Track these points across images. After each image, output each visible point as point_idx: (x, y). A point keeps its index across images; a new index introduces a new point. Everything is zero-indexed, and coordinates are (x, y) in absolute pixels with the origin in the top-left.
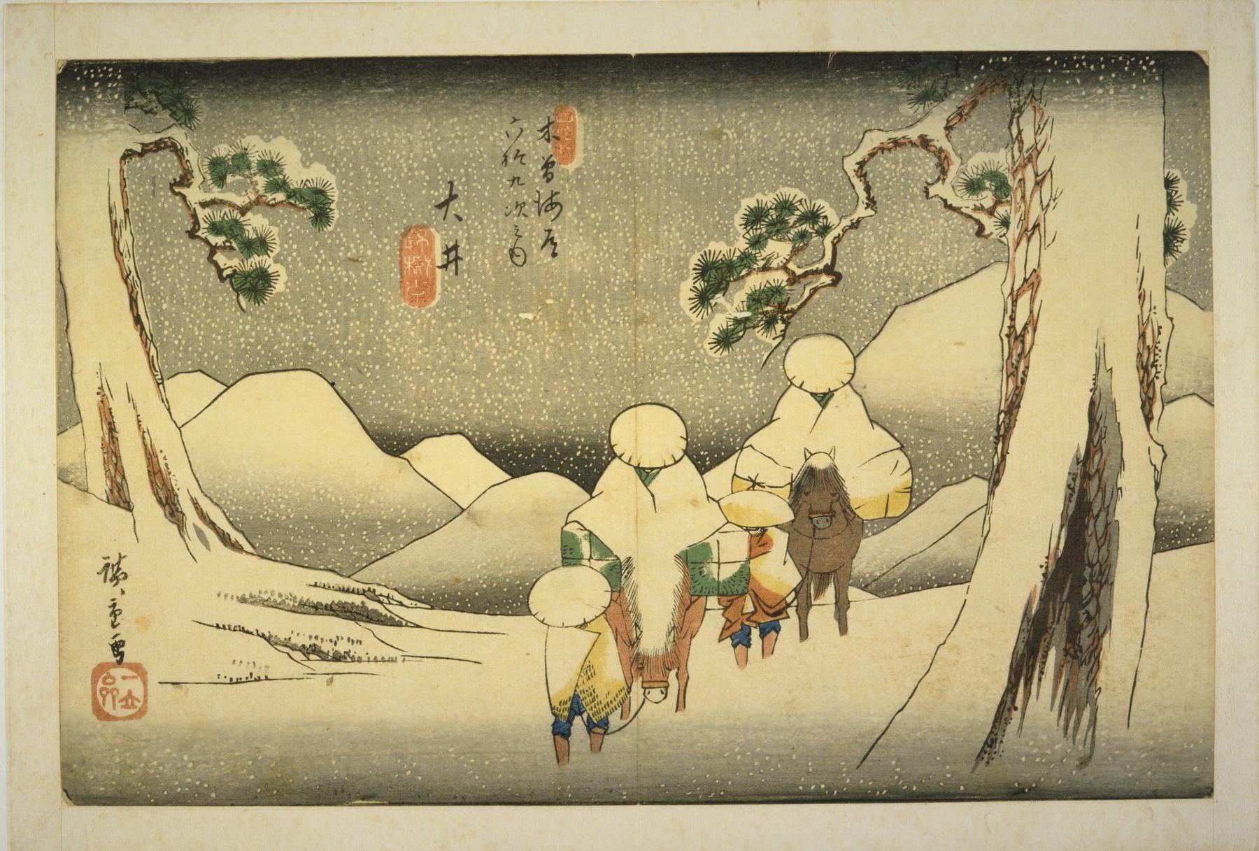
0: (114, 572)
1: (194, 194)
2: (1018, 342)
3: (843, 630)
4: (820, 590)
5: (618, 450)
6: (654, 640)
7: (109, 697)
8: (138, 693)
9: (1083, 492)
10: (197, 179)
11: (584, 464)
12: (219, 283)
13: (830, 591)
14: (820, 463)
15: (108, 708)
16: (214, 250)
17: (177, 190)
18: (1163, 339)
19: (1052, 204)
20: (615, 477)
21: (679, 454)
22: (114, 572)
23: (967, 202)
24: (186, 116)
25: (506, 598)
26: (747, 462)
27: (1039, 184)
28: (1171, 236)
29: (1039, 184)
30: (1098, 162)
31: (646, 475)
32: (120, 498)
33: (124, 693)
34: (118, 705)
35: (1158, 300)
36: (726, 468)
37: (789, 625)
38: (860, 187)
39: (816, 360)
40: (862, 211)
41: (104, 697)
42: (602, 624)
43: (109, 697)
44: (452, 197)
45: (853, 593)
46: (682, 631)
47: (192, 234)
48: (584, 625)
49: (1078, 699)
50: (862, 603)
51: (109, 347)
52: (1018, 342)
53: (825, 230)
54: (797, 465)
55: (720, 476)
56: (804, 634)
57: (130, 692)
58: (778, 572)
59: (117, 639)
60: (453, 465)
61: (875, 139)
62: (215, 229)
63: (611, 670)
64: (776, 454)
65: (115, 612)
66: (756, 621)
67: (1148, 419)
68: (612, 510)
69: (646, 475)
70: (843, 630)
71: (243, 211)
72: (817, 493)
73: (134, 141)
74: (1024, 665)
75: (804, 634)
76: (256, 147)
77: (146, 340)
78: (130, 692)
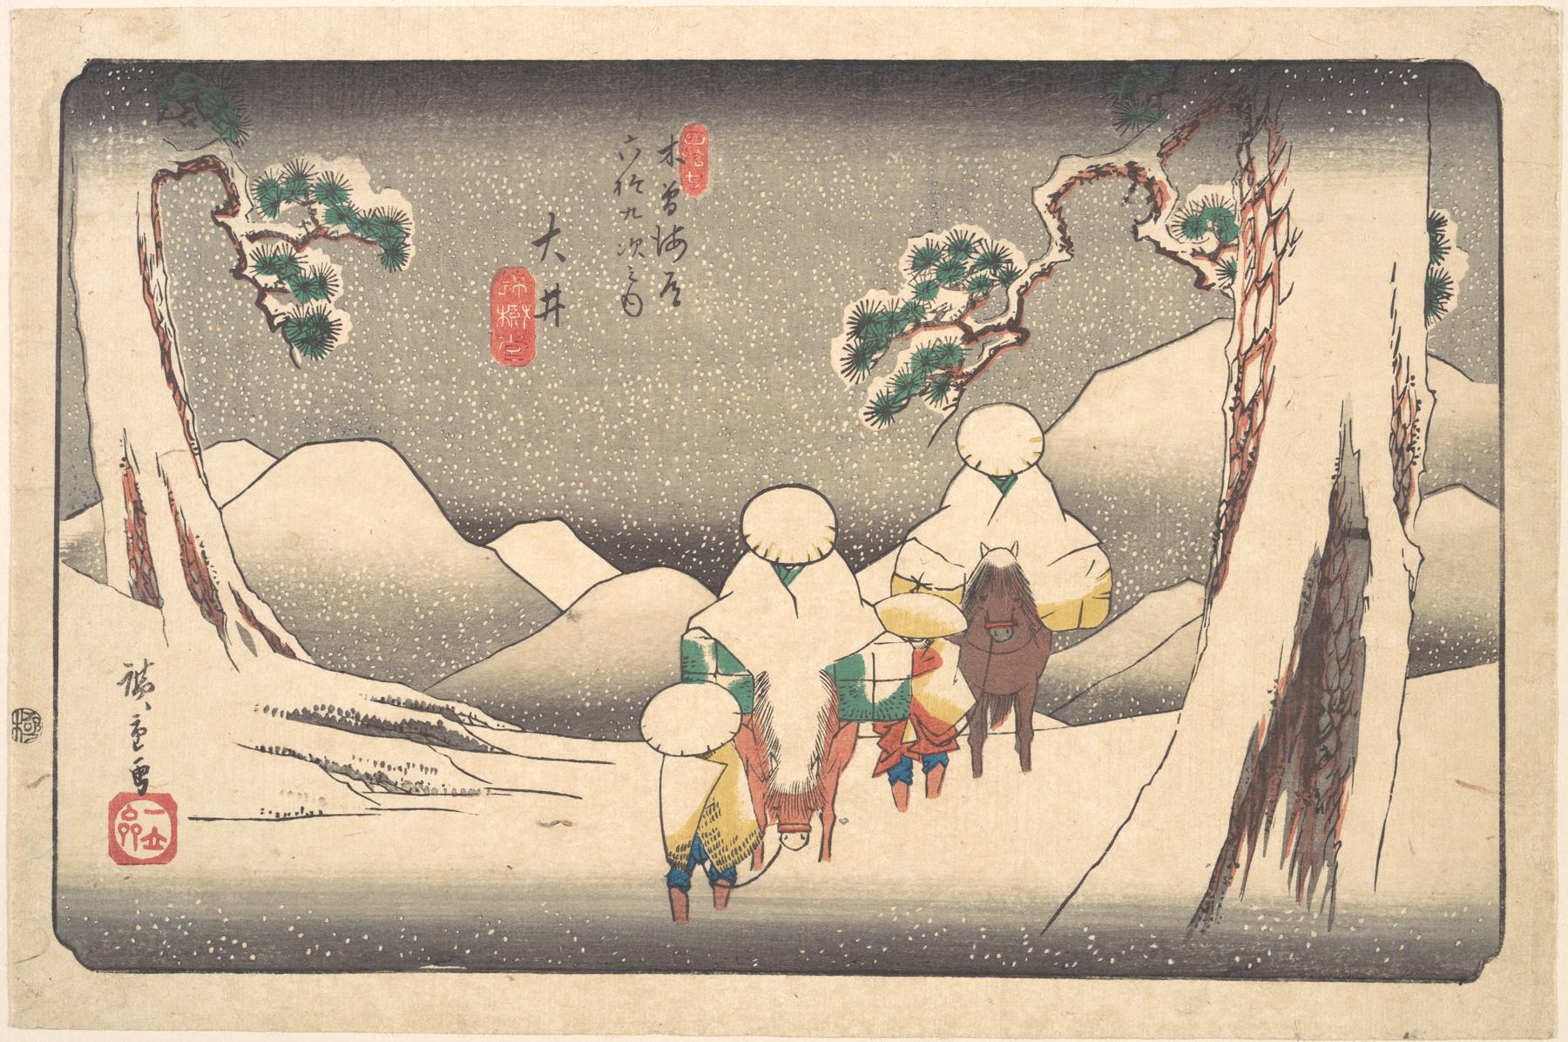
0: (136, 683)
1: (240, 225)
2: (1246, 414)
3: (1026, 765)
4: (999, 718)
5: (751, 542)
6: (792, 773)
7: (130, 836)
8: (165, 831)
9: (1321, 603)
10: (245, 206)
11: (711, 557)
12: (271, 351)
13: (1010, 722)
14: (1001, 561)
15: (128, 849)
16: (263, 292)
17: (220, 219)
18: (1423, 416)
19: (1289, 249)
20: (748, 573)
21: (826, 548)
22: (136, 683)
23: (1184, 247)
24: (232, 131)
25: (612, 717)
26: (911, 559)
27: (1273, 224)
28: (1435, 290)
29: (1273, 224)
30: (1354, 214)
31: (785, 572)
32: (146, 590)
33: (147, 831)
34: (141, 844)
35: (1417, 367)
36: (884, 566)
37: (960, 759)
38: (1053, 223)
39: (997, 433)
40: (1056, 255)
41: (123, 835)
42: (729, 753)
43: (130, 836)
44: (554, 232)
45: (1039, 720)
46: (829, 762)
47: (238, 273)
48: (706, 756)
49: (1314, 851)
50: (1049, 733)
51: (133, 405)
52: (1246, 414)
53: (1010, 276)
54: (972, 563)
55: (876, 576)
56: (978, 770)
57: (155, 829)
58: (947, 693)
59: (141, 764)
60: (548, 556)
61: (1072, 167)
62: (266, 266)
63: (743, 809)
64: (949, 547)
65: (138, 730)
66: (915, 751)
67: (1403, 515)
68: (748, 614)
69: (785, 572)
70: (1026, 765)
71: (299, 245)
72: (996, 595)
73: (172, 158)
74: (1247, 817)
75: (978, 770)
76: (318, 167)
77: (182, 402)
78: (155, 829)
